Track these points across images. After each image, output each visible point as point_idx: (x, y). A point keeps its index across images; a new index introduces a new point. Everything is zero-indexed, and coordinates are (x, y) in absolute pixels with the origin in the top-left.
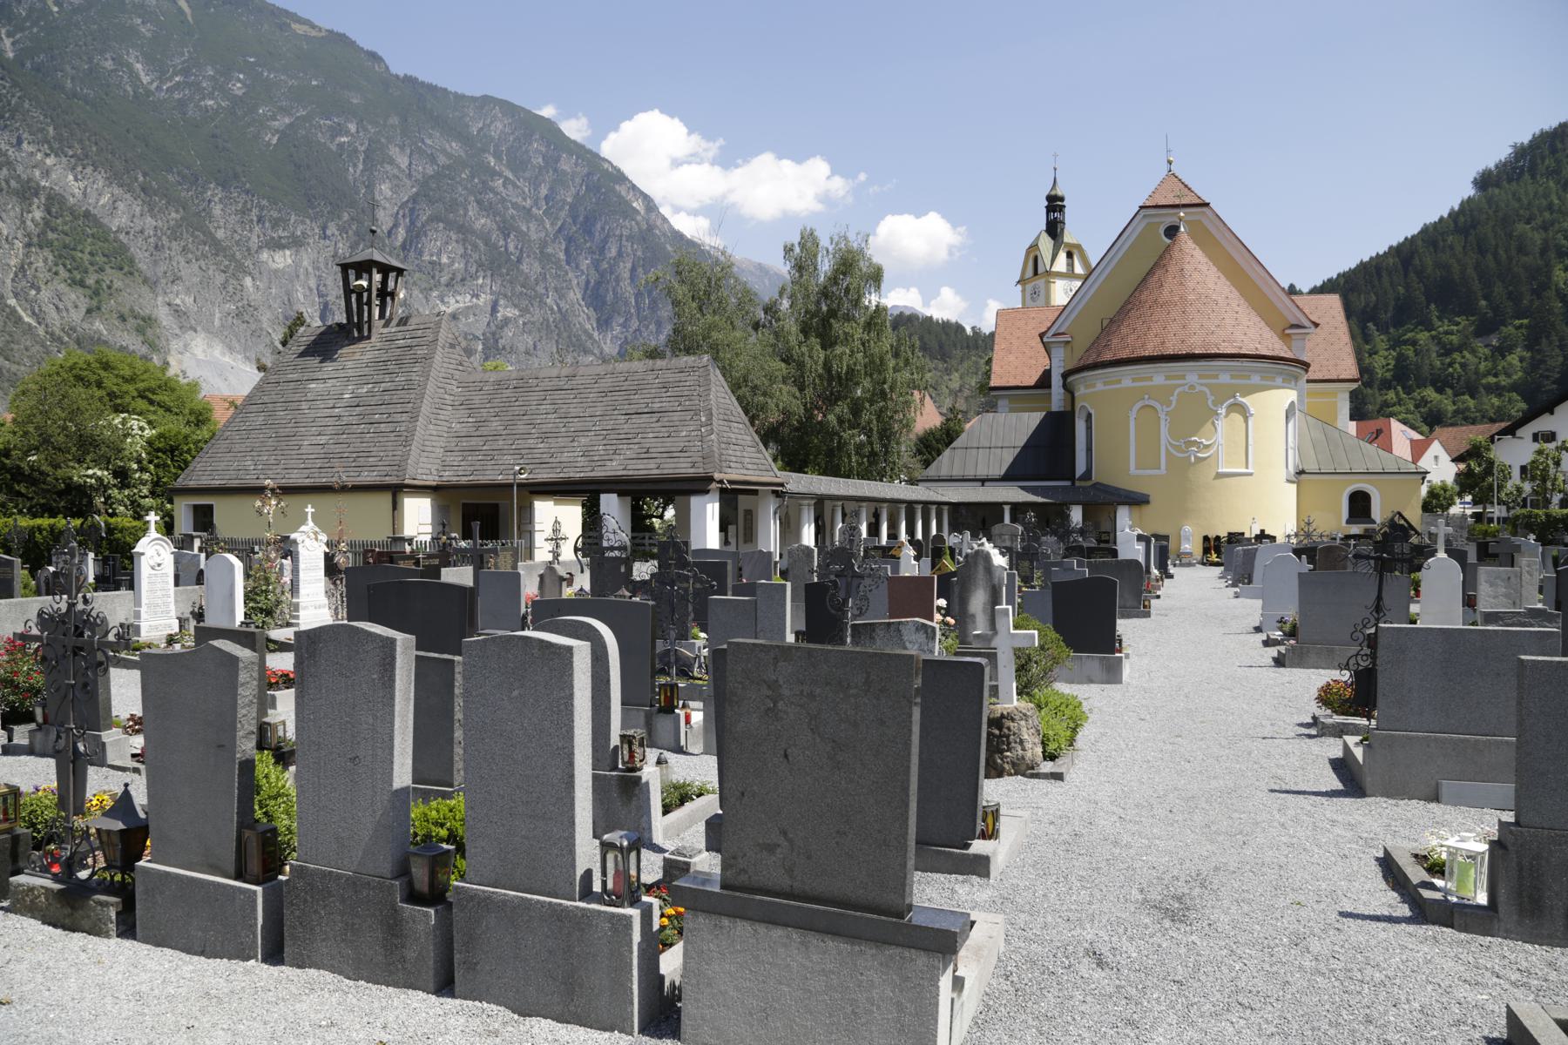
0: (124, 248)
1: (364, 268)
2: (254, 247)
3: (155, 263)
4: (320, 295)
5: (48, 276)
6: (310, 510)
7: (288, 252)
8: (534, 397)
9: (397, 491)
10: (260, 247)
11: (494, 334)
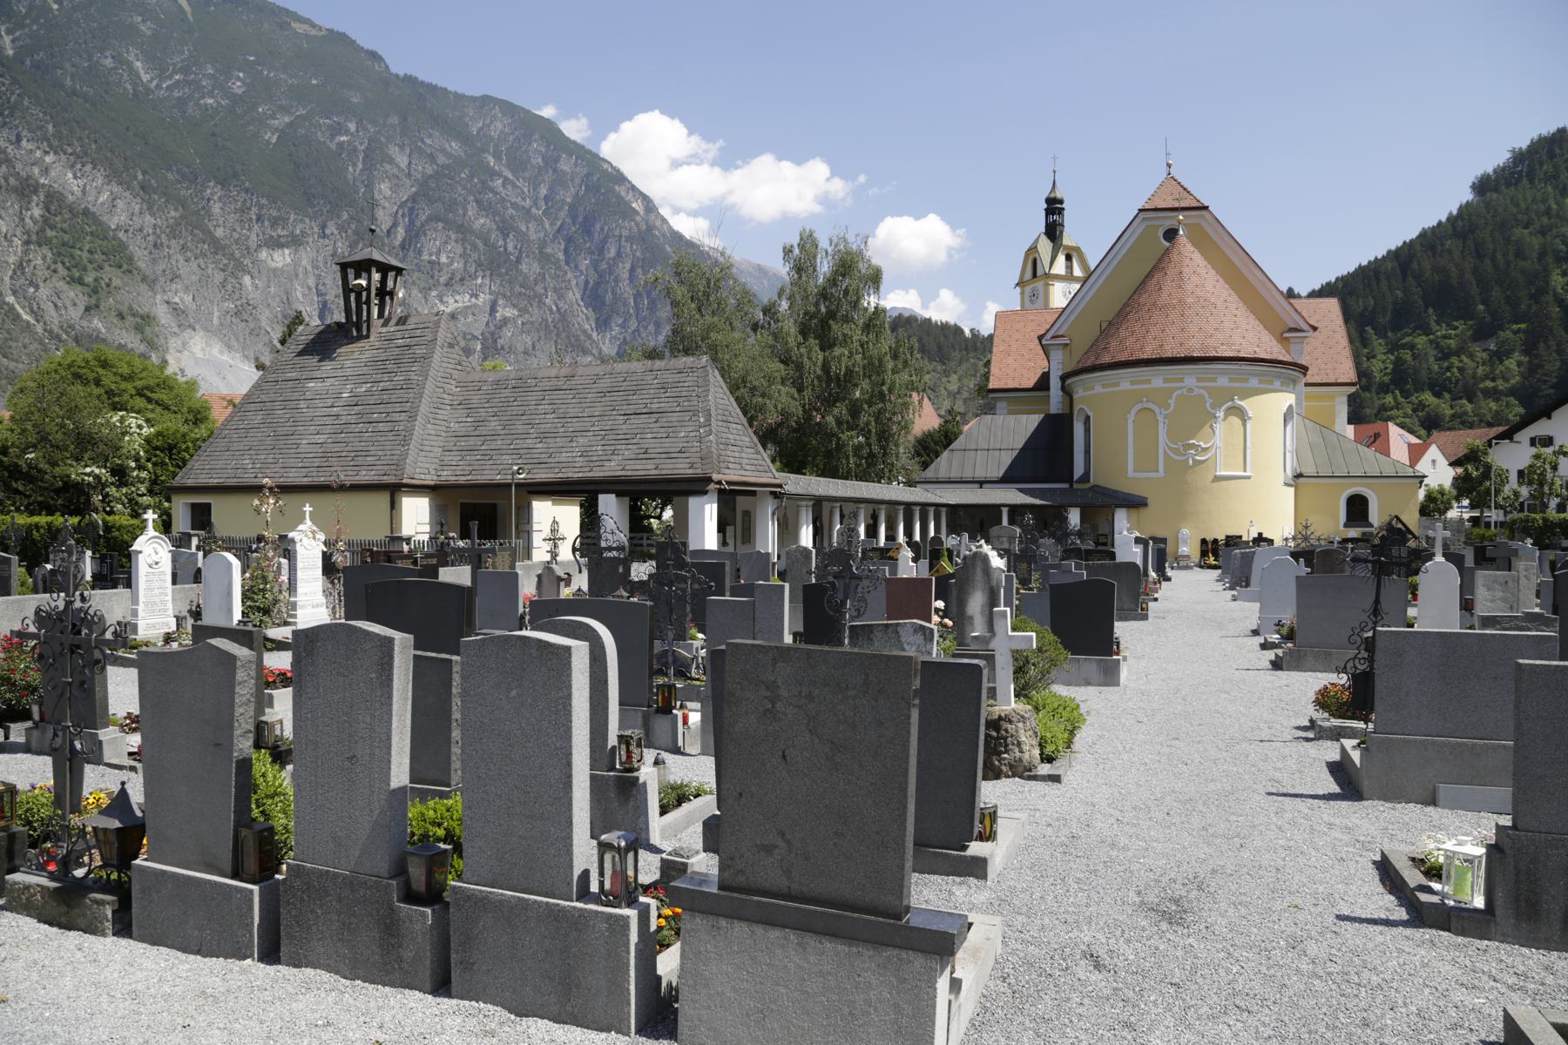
0: (122, 246)
1: (363, 267)
3: (154, 261)
4: (319, 294)
6: (308, 508)
7: (287, 251)
8: (532, 397)
9: (395, 490)
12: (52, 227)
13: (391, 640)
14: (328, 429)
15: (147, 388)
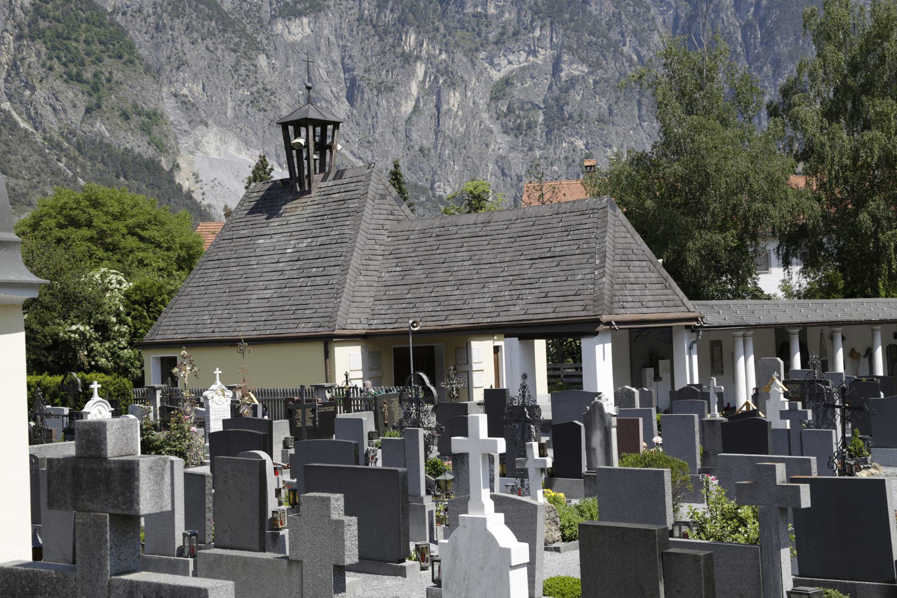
0: (121, 32)
1: (300, 124)
2: (266, 17)
3: (157, 46)
4: (346, 70)
5: (42, 71)
6: (218, 372)
7: (305, 20)
8: (453, 244)
9: (328, 342)
10: (274, 17)
11: (557, 100)
12: (45, 17)
13: (501, 492)
14: (274, 284)
15: (138, 226)
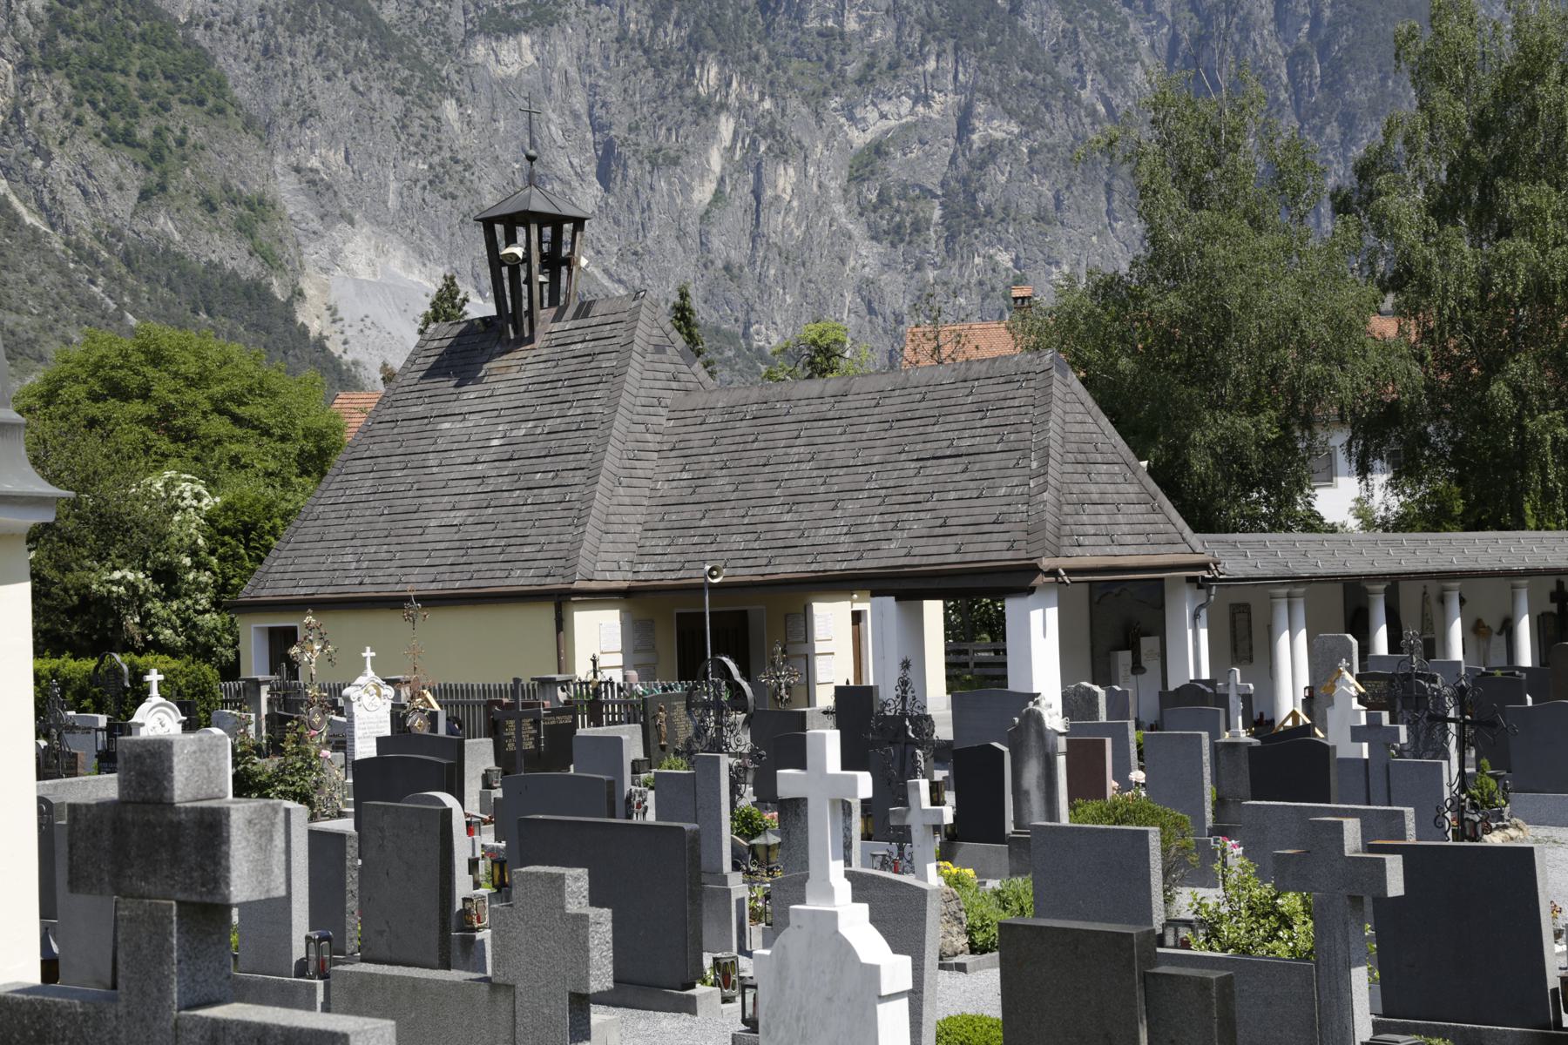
0: (203, 59)
1: (515, 220)
2: (458, 34)
3: (266, 84)
4: (597, 127)
6: (368, 654)
7: (526, 40)
8: (783, 432)
9: (562, 601)
10: (470, 34)
11: (965, 181)
12: (69, 31)
